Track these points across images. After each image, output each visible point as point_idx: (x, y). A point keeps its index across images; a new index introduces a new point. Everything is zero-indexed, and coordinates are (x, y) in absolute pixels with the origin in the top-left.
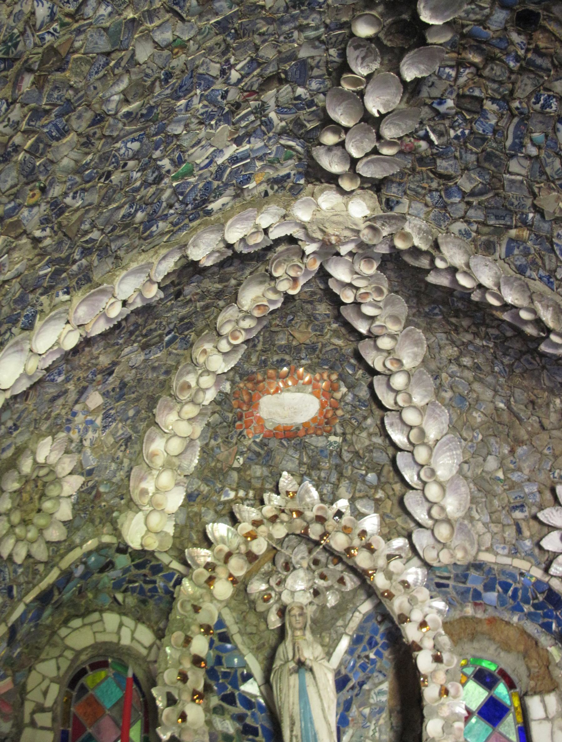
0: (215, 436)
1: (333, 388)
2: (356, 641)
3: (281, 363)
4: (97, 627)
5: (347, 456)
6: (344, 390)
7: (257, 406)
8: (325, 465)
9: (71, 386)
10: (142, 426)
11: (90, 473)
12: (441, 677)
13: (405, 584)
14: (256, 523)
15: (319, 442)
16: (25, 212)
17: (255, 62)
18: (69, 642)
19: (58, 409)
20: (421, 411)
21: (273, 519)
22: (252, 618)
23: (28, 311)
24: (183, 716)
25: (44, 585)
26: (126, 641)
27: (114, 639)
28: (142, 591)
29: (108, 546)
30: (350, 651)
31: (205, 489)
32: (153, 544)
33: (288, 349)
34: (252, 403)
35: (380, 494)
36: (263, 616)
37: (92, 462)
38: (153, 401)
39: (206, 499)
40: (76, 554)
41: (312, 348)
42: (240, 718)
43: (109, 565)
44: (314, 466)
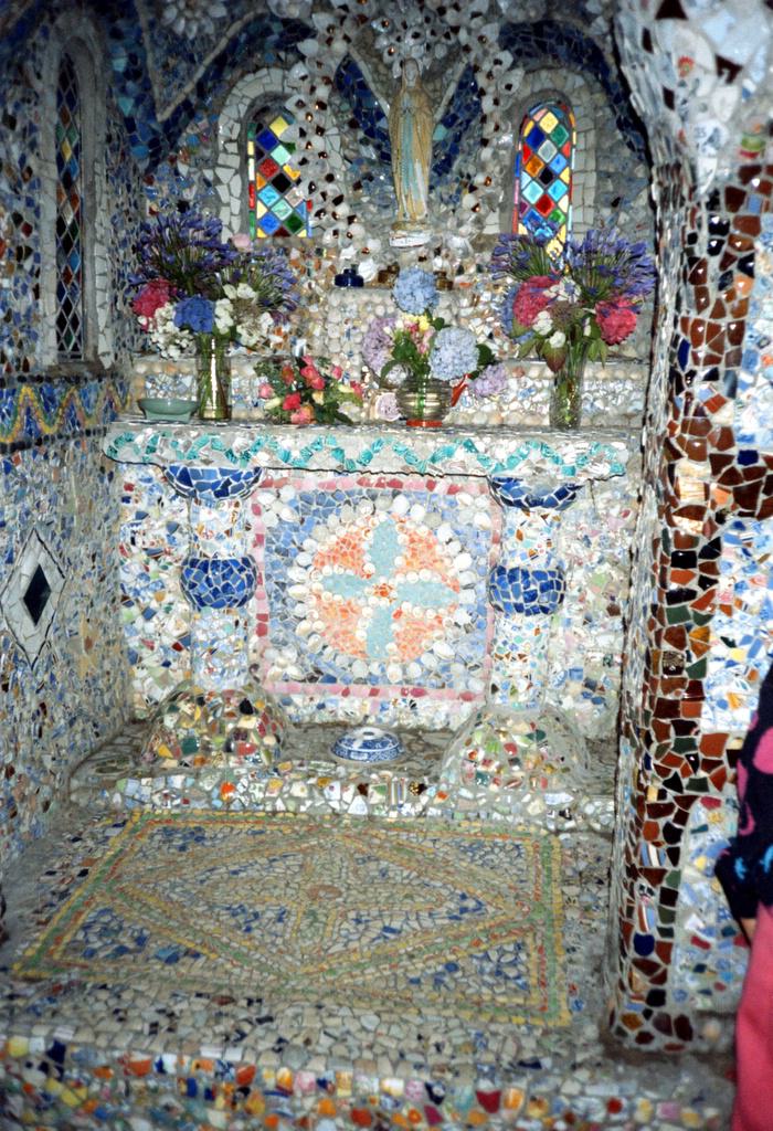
4: (265, 81)
12: (497, 116)
22: (382, 69)
24: (309, 143)
25: (217, 52)
36: (389, 67)
40: (237, 26)
42: (378, 147)
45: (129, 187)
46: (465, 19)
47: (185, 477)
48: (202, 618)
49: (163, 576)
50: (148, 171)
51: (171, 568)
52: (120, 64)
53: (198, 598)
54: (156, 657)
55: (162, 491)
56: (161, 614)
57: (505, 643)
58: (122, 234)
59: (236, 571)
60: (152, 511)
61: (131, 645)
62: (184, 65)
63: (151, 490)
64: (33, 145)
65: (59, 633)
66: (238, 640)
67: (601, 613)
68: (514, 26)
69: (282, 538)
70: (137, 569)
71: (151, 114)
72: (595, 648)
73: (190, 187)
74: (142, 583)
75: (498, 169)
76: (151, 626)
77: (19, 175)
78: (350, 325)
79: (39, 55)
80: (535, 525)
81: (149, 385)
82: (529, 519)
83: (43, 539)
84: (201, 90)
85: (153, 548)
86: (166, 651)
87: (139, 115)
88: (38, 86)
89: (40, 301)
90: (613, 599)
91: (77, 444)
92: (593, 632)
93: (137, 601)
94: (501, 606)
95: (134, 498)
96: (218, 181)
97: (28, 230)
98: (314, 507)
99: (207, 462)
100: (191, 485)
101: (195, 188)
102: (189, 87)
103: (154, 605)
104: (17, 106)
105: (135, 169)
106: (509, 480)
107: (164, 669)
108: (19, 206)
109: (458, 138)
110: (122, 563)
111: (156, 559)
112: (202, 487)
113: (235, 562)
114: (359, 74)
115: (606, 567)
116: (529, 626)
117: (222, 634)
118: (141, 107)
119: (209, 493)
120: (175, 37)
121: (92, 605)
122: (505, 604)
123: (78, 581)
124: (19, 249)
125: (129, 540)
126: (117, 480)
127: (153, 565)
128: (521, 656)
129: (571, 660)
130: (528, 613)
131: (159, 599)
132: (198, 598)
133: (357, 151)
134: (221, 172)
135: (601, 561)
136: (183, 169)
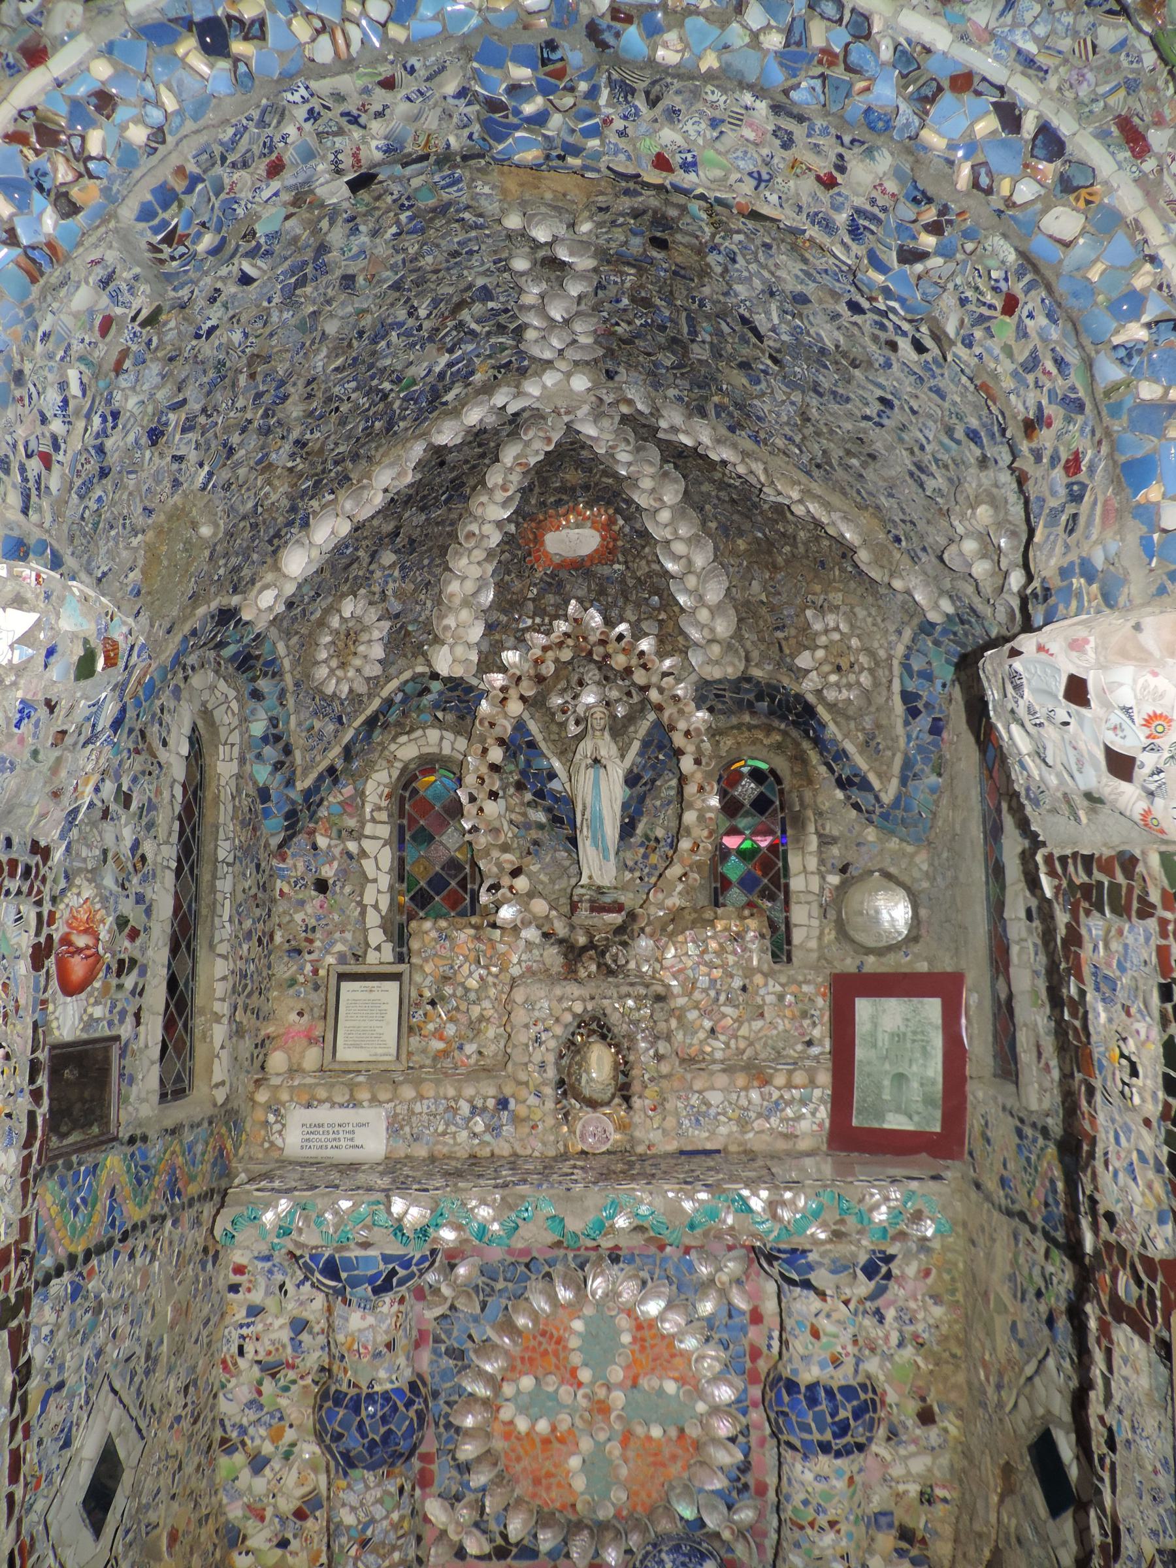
0: (509, 573)
1: (612, 521)
2: (646, 744)
3: (559, 503)
4: (422, 742)
5: (631, 582)
6: (621, 522)
7: (543, 543)
8: (612, 591)
9: (361, 553)
10: (438, 571)
11: (397, 616)
12: (699, 776)
13: (676, 699)
14: (545, 649)
15: (605, 570)
16: (274, 456)
17: (436, 303)
18: (399, 754)
19: (355, 571)
20: (688, 541)
21: (560, 645)
22: (554, 728)
23: (301, 514)
24: (481, 809)
25: (369, 712)
26: (447, 750)
27: (435, 750)
28: (457, 708)
29: (422, 675)
30: (641, 754)
31: (504, 619)
32: (458, 672)
33: (563, 489)
34: (538, 540)
35: (663, 616)
36: (563, 725)
37: (396, 606)
38: (444, 551)
39: (506, 628)
40: (394, 684)
41: (586, 488)
42: (549, 810)
43: (427, 690)
44: (602, 592)
45: (258, 866)
46: (655, 679)
47: (331, 1269)
48: (349, 1486)
49: (283, 1402)
50: (280, 846)
51: (293, 1388)
52: (258, 728)
53: (346, 1456)
54: (267, 1533)
55: (285, 1273)
56: (276, 1464)
57: (806, 1503)
58: (248, 924)
59: (402, 1408)
60: (271, 1304)
61: (231, 1516)
62: (331, 727)
63: (270, 1272)
64: (150, 826)
65: (130, 1536)
66: (402, 1518)
67: (909, 1423)
68: (707, 683)
69: (455, 1333)
70: (244, 1393)
71: (290, 783)
72: (908, 1477)
73: (330, 863)
74: (252, 1415)
75: (705, 833)
76: (260, 1484)
77: (130, 865)
78: (540, 1027)
79: (167, 717)
80: (835, 1316)
81: (271, 1118)
82: (826, 1307)
83: (117, 1387)
84: (348, 753)
85: (270, 1359)
86: (283, 1521)
87: (275, 784)
88: (163, 755)
89: (142, 1028)
90: (923, 1399)
91: (174, 1224)
92: (902, 1452)
93: (243, 1443)
94: (798, 1444)
95: (246, 1285)
96: (363, 853)
97: (134, 935)
98: (500, 1285)
99: (365, 1245)
100: (339, 1279)
101: (335, 864)
102: (336, 751)
103: (267, 1448)
104: (135, 780)
105: (267, 845)
106: (794, 1251)
107: (279, 1552)
108: (127, 907)
109: (642, 799)
110: (223, 1386)
111: (273, 1376)
112: (354, 1283)
113: (399, 1391)
114: (528, 733)
115: (909, 1351)
116: (839, 1473)
117: (379, 1512)
118: (278, 775)
119: (366, 1290)
120: (324, 697)
121: (180, 1468)
122: (803, 1441)
123: (163, 1435)
124: (121, 962)
125: (234, 1349)
126: (222, 1260)
127: (268, 1386)
128: (832, 1524)
129: (876, 1499)
130: (838, 1454)
131: (276, 1438)
132: (346, 1456)
133: (524, 814)
134: (367, 845)
135: (901, 1344)
136: (322, 842)
